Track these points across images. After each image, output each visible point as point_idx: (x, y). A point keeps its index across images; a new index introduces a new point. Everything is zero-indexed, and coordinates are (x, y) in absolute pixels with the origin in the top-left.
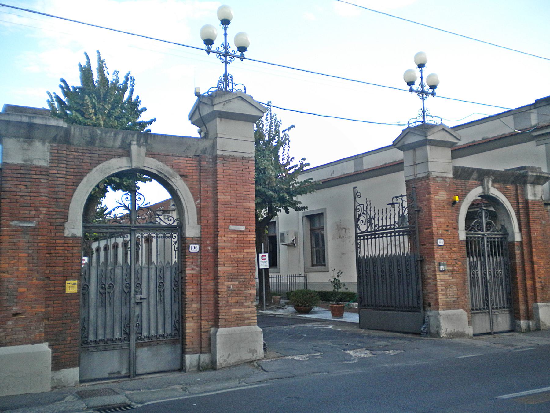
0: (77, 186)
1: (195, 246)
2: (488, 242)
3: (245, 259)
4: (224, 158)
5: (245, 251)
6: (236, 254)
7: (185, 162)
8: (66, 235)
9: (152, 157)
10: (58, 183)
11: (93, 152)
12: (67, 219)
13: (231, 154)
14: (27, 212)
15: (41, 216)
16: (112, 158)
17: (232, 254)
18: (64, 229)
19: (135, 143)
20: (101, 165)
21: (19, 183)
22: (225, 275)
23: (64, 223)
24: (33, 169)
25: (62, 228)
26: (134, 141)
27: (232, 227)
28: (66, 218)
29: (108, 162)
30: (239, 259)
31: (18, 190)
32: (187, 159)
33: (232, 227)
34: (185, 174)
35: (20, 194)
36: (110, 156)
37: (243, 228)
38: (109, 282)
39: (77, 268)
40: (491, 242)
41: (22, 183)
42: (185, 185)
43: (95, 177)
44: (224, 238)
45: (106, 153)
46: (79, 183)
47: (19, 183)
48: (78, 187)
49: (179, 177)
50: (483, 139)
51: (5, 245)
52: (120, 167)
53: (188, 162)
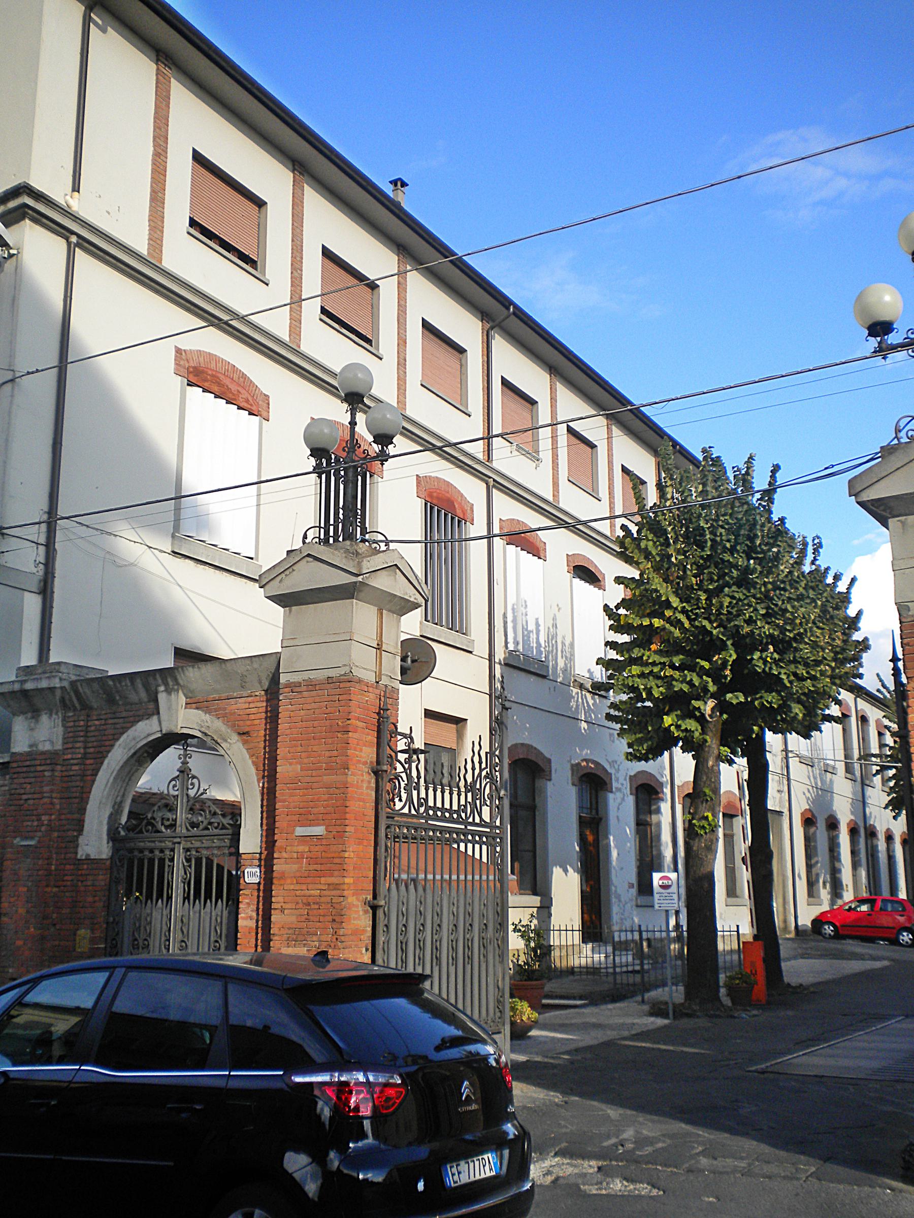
0: (96, 775)
1: (254, 870)
2: (188, 860)
3: (323, 899)
4: (293, 687)
5: (323, 880)
6: (304, 887)
7: (247, 706)
8: (79, 857)
9: (197, 708)
10: (71, 773)
11: (118, 715)
12: (82, 830)
13: (306, 676)
14: (29, 823)
15: (43, 829)
16: (138, 721)
17: (298, 887)
18: (77, 846)
19: (162, 688)
20: (125, 736)
21: (22, 781)
22: (283, 931)
23: (77, 837)
24: (38, 757)
25: (72, 845)
26: (159, 686)
27: (300, 831)
28: (80, 830)
29: (133, 728)
30: (310, 900)
31: (22, 791)
32: (250, 699)
33: (300, 831)
34: (246, 729)
35: (24, 797)
36: (137, 719)
37: (319, 830)
38: (143, 936)
39: (90, 910)
40: (199, 861)
41: (27, 780)
42: (245, 751)
43: (117, 755)
44: (284, 855)
45: (132, 713)
46: (98, 770)
47: (22, 781)
48: (98, 778)
49: (235, 737)
50: (55, 550)
51: (7, 874)
52: (149, 735)
53: (252, 705)
